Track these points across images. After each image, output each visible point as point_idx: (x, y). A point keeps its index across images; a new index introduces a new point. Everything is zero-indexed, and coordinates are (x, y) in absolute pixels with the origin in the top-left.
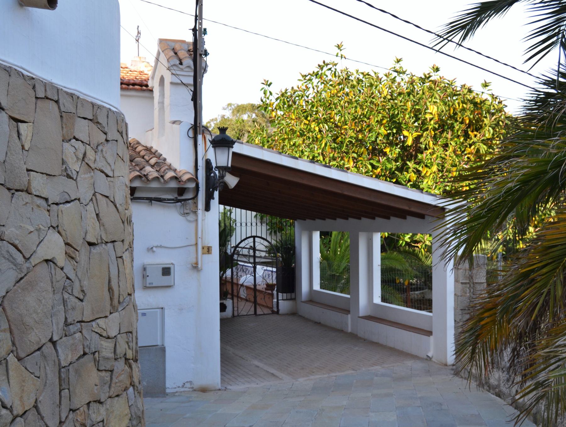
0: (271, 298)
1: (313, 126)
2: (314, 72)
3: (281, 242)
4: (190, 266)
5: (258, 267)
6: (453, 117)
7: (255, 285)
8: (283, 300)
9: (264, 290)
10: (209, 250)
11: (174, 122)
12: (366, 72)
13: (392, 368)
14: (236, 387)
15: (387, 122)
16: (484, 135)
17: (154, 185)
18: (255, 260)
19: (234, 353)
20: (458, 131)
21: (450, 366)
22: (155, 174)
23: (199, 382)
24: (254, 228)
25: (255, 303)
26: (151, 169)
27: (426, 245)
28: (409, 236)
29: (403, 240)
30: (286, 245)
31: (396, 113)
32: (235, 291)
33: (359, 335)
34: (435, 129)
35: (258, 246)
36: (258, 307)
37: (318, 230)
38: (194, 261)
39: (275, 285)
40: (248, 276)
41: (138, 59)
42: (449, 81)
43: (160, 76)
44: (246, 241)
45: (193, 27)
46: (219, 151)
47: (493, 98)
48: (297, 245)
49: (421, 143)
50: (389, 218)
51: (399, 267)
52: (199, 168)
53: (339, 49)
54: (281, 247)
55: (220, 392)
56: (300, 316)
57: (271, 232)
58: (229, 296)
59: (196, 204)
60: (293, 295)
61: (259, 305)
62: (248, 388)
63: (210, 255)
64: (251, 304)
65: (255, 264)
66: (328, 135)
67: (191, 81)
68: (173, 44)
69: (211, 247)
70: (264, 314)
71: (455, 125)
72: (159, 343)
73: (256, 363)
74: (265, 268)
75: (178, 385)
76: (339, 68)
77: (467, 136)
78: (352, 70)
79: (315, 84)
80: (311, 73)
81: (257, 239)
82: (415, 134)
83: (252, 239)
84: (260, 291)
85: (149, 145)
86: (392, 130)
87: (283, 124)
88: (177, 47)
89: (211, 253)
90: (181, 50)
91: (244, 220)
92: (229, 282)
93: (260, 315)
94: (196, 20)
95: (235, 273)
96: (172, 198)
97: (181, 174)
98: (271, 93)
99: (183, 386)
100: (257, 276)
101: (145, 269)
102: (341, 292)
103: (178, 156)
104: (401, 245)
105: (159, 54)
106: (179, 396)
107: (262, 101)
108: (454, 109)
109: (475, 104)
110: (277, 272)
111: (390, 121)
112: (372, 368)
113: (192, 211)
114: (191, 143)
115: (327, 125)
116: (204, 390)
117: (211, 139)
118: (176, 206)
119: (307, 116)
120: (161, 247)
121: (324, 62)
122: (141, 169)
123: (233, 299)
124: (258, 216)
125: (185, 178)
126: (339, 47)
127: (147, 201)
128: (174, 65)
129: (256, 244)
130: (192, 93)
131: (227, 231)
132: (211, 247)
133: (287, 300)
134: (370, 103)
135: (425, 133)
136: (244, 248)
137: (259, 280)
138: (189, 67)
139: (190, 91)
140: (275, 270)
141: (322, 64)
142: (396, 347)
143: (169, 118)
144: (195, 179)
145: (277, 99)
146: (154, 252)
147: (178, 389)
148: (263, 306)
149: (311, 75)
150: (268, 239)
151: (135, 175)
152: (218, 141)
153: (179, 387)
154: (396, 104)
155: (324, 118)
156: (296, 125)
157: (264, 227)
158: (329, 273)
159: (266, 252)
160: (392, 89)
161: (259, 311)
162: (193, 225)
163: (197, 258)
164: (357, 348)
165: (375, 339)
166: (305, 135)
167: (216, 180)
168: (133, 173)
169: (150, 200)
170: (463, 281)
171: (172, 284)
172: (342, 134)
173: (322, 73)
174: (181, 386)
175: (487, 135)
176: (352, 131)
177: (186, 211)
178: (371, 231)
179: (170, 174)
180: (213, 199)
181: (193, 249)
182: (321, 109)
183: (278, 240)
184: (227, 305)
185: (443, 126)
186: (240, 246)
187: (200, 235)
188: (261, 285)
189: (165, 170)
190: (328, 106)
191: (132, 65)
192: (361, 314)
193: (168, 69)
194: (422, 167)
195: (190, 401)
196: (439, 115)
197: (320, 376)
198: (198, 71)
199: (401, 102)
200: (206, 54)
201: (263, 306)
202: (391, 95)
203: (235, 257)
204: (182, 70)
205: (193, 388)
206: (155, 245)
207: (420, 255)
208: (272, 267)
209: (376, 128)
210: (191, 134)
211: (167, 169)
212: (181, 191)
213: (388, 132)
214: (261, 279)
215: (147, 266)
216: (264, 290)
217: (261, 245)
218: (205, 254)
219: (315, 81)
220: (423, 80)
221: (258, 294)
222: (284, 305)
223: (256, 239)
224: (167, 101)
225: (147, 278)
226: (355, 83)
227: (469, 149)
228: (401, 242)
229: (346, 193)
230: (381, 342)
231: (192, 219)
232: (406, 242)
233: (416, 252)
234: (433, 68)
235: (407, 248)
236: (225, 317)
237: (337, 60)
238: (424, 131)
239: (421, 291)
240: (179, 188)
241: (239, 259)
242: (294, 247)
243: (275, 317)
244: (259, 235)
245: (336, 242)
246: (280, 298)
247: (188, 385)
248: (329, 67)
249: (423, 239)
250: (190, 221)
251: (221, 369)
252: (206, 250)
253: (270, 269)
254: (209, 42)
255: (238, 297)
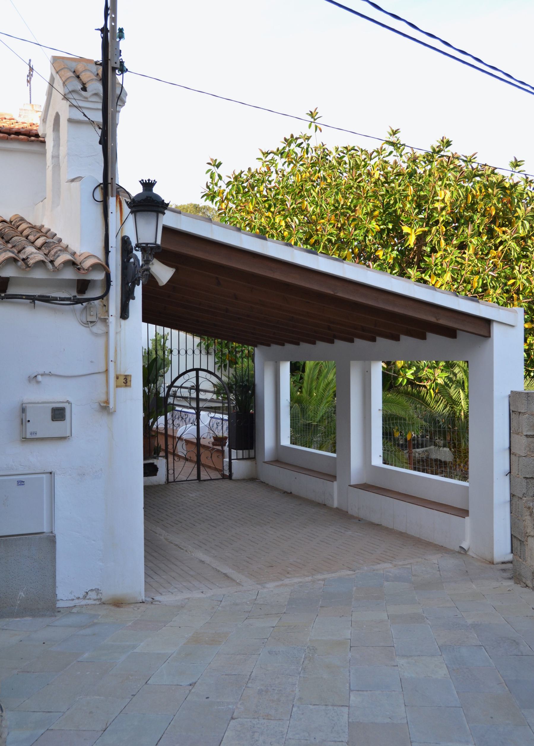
0: (221, 457)
1: (277, 220)
2: (278, 150)
3: (235, 377)
4: (96, 406)
5: (202, 413)
6: (472, 207)
7: (198, 438)
8: (237, 459)
9: (211, 445)
10: (126, 381)
11: (73, 181)
12: (351, 146)
13: (409, 566)
14: (167, 599)
15: (380, 213)
16: (517, 232)
17: (38, 274)
18: (198, 404)
19: (167, 539)
20: (478, 227)
21: (498, 564)
22: (40, 256)
23: (110, 591)
24: (197, 357)
25: (198, 463)
26: (34, 250)
27: (437, 384)
28: (412, 371)
29: (404, 377)
30: (243, 382)
31: (392, 202)
32: (170, 447)
33: (350, 512)
34: (447, 224)
35: (204, 385)
36: (202, 468)
37: (287, 360)
38: (103, 397)
39: (226, 438)
40: (188, 425)
41: (29, 107)
42: (466, 157)
43: (54, 114)
44: (186, 376)
45: (101, 25)
46: (141, 222)
47: (527, 182)
48: (257, 381)
49: (425, 245)
50: (397, 339)
51: (402, 414)
52: (110, 249)
53: (312, 117)
54: (236, 384)
55: (143, 607)
56: (262, 482)
57: (220, 366)
58: (162, 454)
59: (106, 306)
60: (252, 452)
61: (204, 466)
62: (188, 599)
63: (128, 389)
64: (193, 465)
65: (198, 410)
66: (298, 231)
67: (98, 117)
68: (73, 65)
69: (130, 376)
70: (211, 479)
71: (475, 217)
72: (46, 529)
73: (201, 555)
74: (212, 415)
75: (77, 596)
76: (313, 143)
77: (491, 233)
78: (331, 147)
79: (280, 166)
80: (275, 150)
81: (201, 373)
82: (419, 231)
83: (194, 373)
84: (204, 447)
85: (38, 224)
86: (386, 224)
87: (236, 217)
88: (80, 67)
89: (130, 386)
90: (86, 70)
91: (182, 346)
92: (161, 433)
93: (204, 480)
94: (106, 15)
95: (170, 422)
96: (68, 296)
97: (82, 258)
98: (220, 177)
99: (85, 597)
100: (201, 425)
101: (23, 410)
102: (320, 448)
103: (76, 229)
104: (401, 384)
105: (52, 79)
106: (78, 613)
107: (208, 187)
108: (474, 197)
109: (504, 189)
110: (229, 420)
111: (384, 212)
112: (378, 567)
113: (100, 319)
114: (98, 209)
115: (297, 217)
116: (118, 603)
117: (129, 200)
118: (74, 311)
119: (270, 206)
120: (50, 374)
121: (292, 136)
122: (19, 252)
123: (166, 457)
124: (202, 344)
125: (87, 264)
126: (311, 114)
127: (29, 301)
128: (73, 91)
129: (200, 380)
130: (100, 132)
131: (160, 361)
132: (130, 376)
133: (243, 459)
134: (356, 188)
135: (434, 228)
136: (181, 387)
137: (204, 431)
138: (96, 94)
139: (97, 129)
140: (226, 417)
141: (288, 137)
142: (408, 532)
143: (66, 174)
144: (104, 267)
145: (228, 184)
146: (38, 382)
147: (76, 602)
148: (210, 467)
149: (275, 154)
150: (217, 373)
151: (7, 256)
152: (140, 202)
153: (78, 598)
154: (393, 188)
155: (293, 208)
156: (255, 218)
157: (211, 358)
158: (302, 421)
159: (214, 392)
160: (386, 171)
161: (204, 475)
162: (101, 341)
163: (107, 393)
164: (349, 533)
165: (375, 519)
166: (268, 232)
167: (138, 268)
168: (3, 254)
169: (33, 299)
170: (529, 433)
171: (68, 434)
172: (317, 230)
173: (289, 150)
174: (81, 596)
175: (521, 231)
176: (331, 226)
177: (90, 319)
178: (368, 359)
179: (64, 257)
180: (134, 298)
181: (102, 377)
182: (288, 197)
183: (231, 376)
184: (158, 466)
185: (458, 220)
186: (175, 384)
187: (112, 357)
188: (207, 439)
189: (56, 252)
190: (299, 192)
191: (20, 116)
192: (354, 480)
193: (65, 98)
194: (430, 276)
195: (95, 624)
196: (452, 204)
197: (300, 580)
198: (110, 100)
199: (400, 185)
200: (123, 69)
201: (210, 467)
202: (386, 178)
203: (170, 400)
204: (86, 99)
205: (101, 599)
206: (41, 371)
207: (428, 398)
208: (223, 414)
209: (366, 220)
210: (99, 196)
211: (60, 250)
212: (83, 286)
213: (382, 227)
214: (207, 430)
215: (27, 405)
216: (211, 445)
217: (207, 383)
218: (121, 386)
219: (280, 161)
220: (429, 158)
221: (202, 450)
222: (240, 468)
223: (200, 372)
224: (63, 150)
225: (28, 424)
226: (334, 162)
227: (495, 252)
228: (401, 380)
229: (340, 294)
230: (385, 523)
231: (100, 332)
232: (408, 379)
233: (422, 393)
234: (442, 141)
235: (410, 389)
236: (156, 483)
237: (310, 132)
238: (433, 225)
239: (425, 449)
240: (79, 281)
241: (175, 403)
242: (254, 385)
243: (226, 484)
244: (204, 367)
245: (312, 378)
246: (234, 456)
247: (93, 595)
248: (299, 141)
249: (434, 375)
250: (96, 335)
251: (146, 565)
252: (122, 380)
253: (220, 416)
254: (128, 50)
255: (174, 454)
